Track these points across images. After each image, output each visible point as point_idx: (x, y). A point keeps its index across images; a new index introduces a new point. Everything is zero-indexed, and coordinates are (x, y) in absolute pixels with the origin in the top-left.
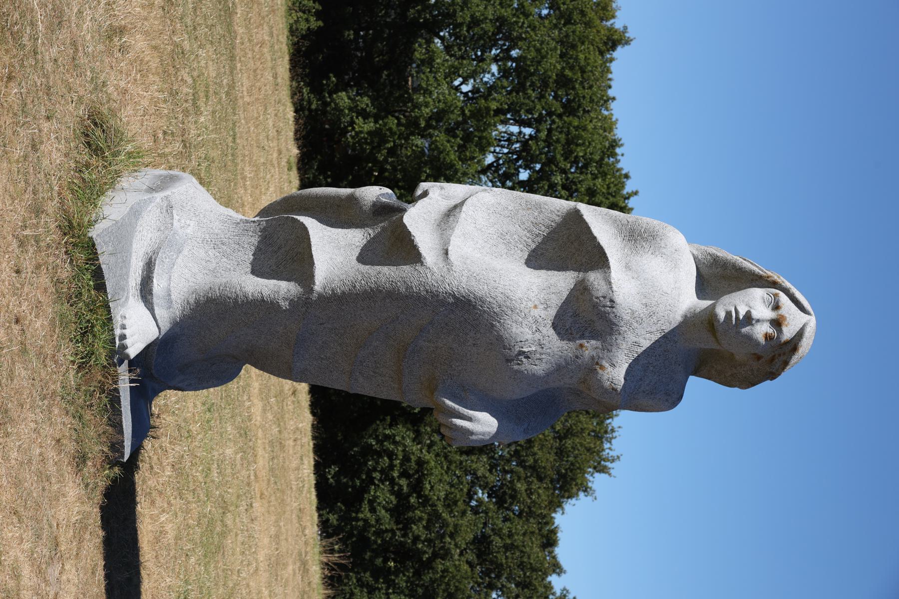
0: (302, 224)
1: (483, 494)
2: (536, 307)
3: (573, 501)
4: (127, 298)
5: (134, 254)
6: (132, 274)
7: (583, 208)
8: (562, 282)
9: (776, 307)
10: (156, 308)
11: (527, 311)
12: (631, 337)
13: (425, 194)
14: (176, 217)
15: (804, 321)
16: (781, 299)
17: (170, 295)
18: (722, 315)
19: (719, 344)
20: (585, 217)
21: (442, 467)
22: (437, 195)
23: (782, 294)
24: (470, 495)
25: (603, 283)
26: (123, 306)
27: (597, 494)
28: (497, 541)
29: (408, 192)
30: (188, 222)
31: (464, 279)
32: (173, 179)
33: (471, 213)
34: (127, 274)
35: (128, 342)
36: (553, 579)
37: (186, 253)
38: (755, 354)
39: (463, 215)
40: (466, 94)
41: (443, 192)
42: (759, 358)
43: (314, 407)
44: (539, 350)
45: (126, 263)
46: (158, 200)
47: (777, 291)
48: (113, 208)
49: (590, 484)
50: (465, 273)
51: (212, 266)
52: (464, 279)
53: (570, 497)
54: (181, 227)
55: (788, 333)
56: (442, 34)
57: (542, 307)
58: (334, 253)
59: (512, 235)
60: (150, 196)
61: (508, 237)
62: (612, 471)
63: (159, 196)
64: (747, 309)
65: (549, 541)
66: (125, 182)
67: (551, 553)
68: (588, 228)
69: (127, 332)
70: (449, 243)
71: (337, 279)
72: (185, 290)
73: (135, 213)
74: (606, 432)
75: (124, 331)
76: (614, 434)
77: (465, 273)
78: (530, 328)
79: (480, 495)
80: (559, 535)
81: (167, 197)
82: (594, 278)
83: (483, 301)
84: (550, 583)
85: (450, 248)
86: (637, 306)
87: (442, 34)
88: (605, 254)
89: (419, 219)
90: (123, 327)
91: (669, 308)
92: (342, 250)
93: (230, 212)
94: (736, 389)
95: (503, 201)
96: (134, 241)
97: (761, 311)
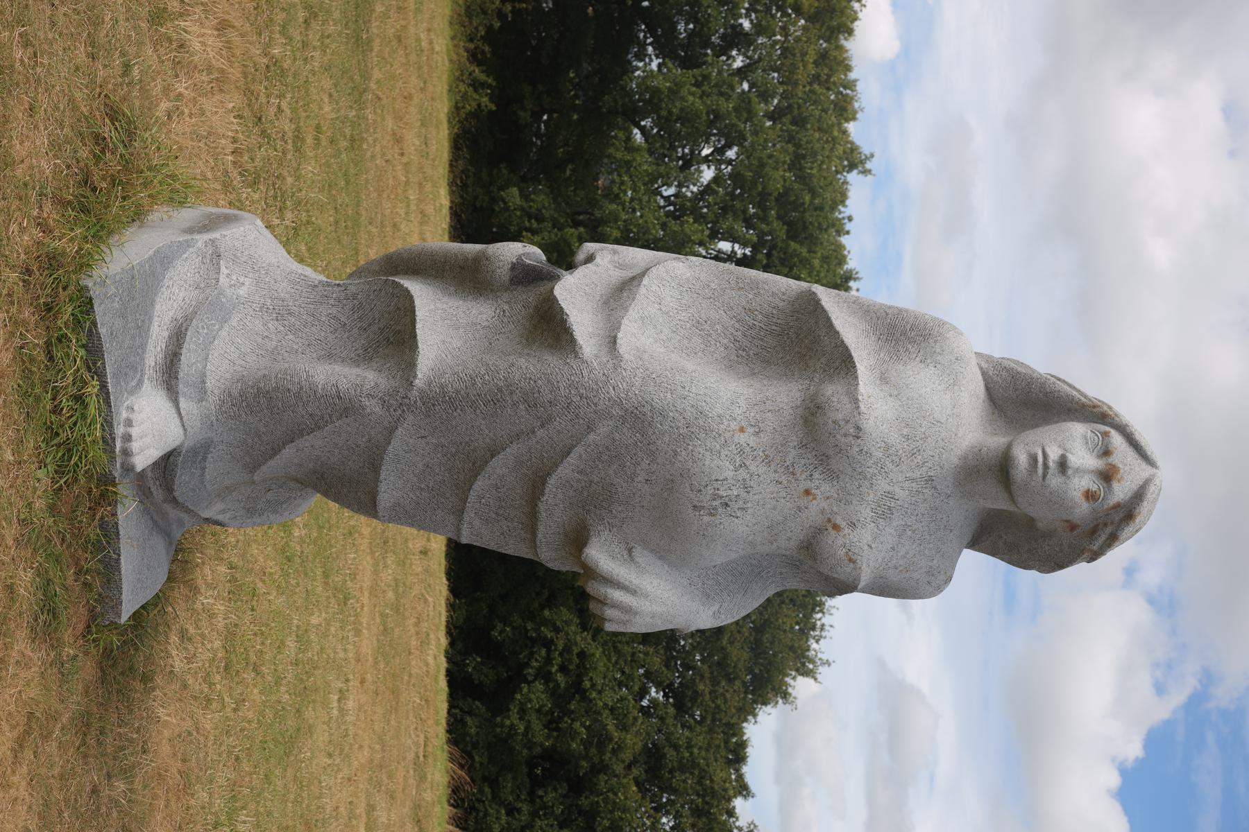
0: (407, 290)
1: (657, 692)
2: (742, 430)
3: (768, 709)
4: (140, 383)
5: (156, 319)
6: (150, 346)
7: (819, 289)
8: (785, 395)
9: (1106, 453)
10: (182, 400)
11: (728, 435)
12: (882, 485)
13: (590, 259)
14: (224, 270)
15: (1145, 475)
16: (1113, 441)
17: (204, 382)
18: (1021, 458)
19: (1014, 502)
20: (823, 303)
21: (609, 660)
22: (605, 262)
23: (1113, 433)
24: (644, 692)
25: (845, 399)
26: (131, 393)
27: (798, 702)
28: (670, 753)
29: (563, 258)
30: (242, 279)
31: (638, 382)
32: (228, 220)
33: (654, 288)
34: (143, 346)
35: (135, 446)
36: (738, 803)
37: (235, 324)
38: (1067, 521)
39: (642, 290)
40: (667, 198)
41: (616, 258)
42: (1073, 527)
43: (454, 575)
44: (743, 495)
45: (142, 330)
46: (200, 244)
47: (1107, 429)
48: (130, 251)
49: (790, 690)
50: (639, 373)
51: (271, 345)
52: (638, 382)
53: (765, 703)
54: (231, 286)
55: (1121, 491)
56: (643, 123)
57: (751, 430)
58: (447, 330)
59: (713, 325)
60: (188, 237)
61: (707, 327)
62: (818, 676)
63: (201, 239)
64: (1060, 452)
65: (738, 755)
66: (158, 214)
67: (737, 770)
68: (828, 319)
69: (134, 432)
70: (619, 328)
71: (449, 371)
72: (228, 376)
73: (163, 260)
74: (814, 628)
75: (129, 430)
76: (823, 634)
77: (639, 373)
78: (732, 461)
79: (653, 694)
80: (749, 750)
81: (213, 241)
82: (833, 391)
83: (662, 414)
84: (734, 808)
85: (620, 335)
86: (894, 438)
87: (643, 123)
88: (850, 356)
89: (575, 293)
90: (129, 423)
91: (941, 444)
92: (461, 330)
93: (309, 272)
94: (1034, 572)
95: (703, 275)
96: (158, 300)
97: (1083, 458)
